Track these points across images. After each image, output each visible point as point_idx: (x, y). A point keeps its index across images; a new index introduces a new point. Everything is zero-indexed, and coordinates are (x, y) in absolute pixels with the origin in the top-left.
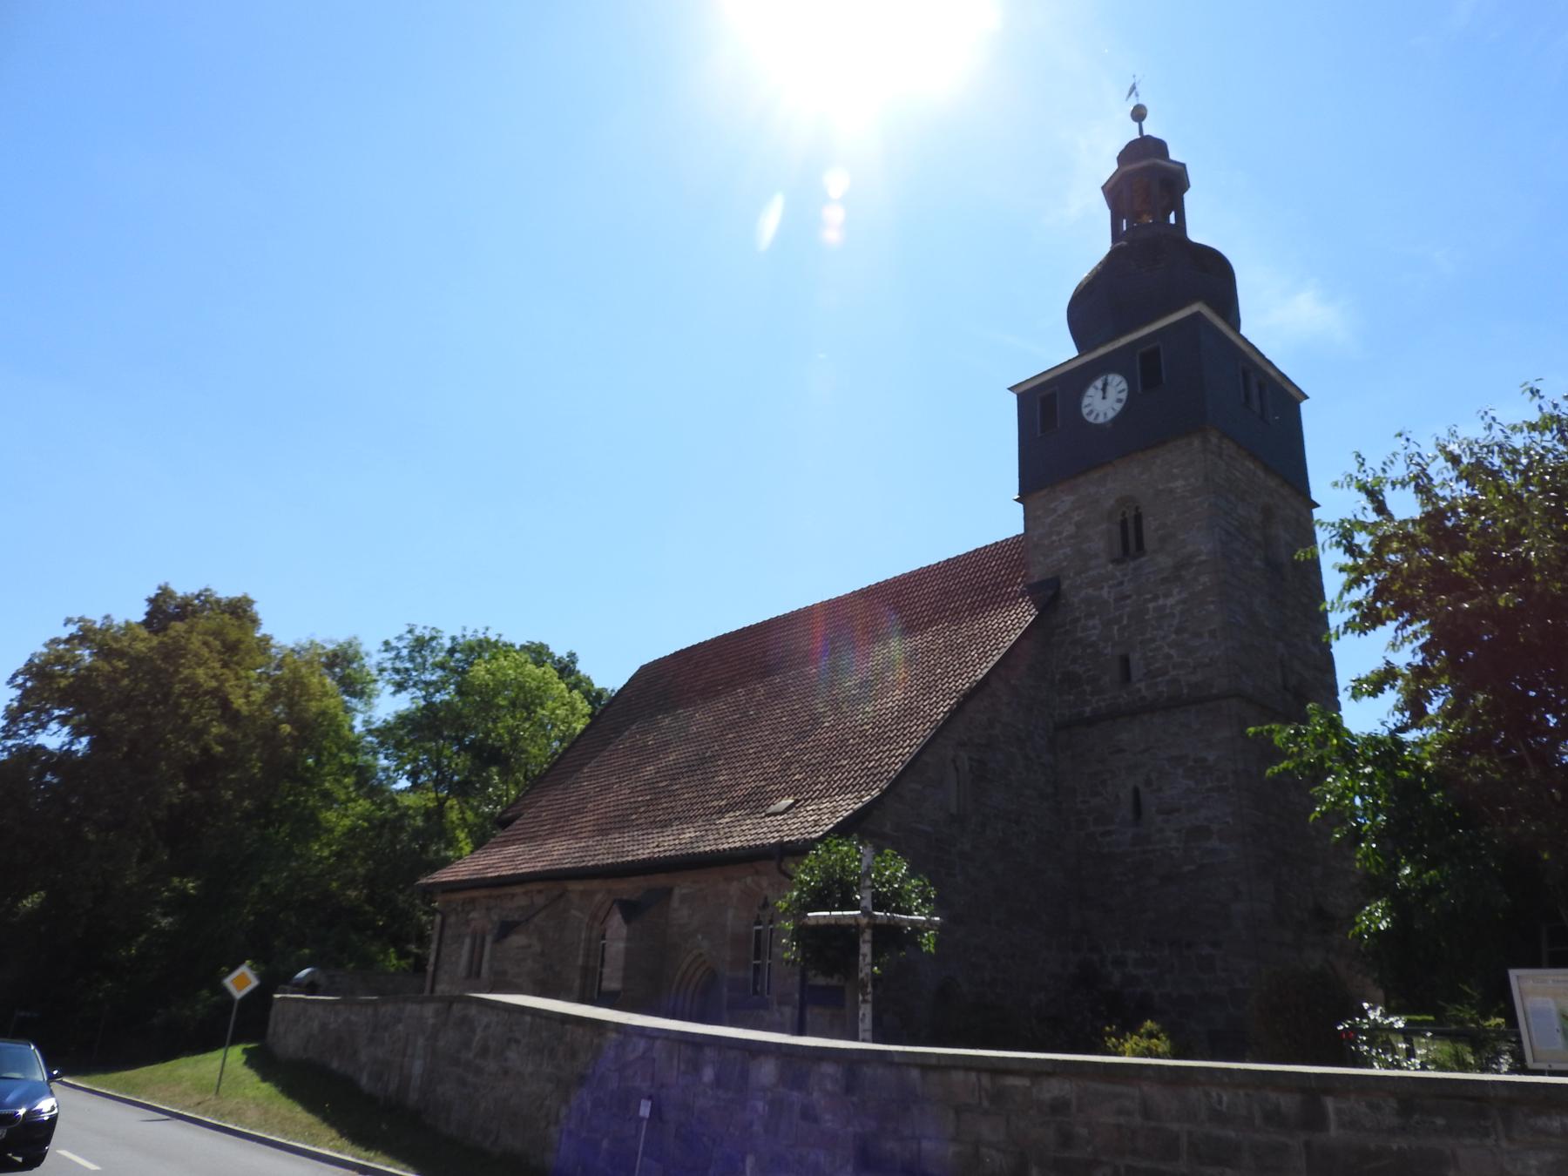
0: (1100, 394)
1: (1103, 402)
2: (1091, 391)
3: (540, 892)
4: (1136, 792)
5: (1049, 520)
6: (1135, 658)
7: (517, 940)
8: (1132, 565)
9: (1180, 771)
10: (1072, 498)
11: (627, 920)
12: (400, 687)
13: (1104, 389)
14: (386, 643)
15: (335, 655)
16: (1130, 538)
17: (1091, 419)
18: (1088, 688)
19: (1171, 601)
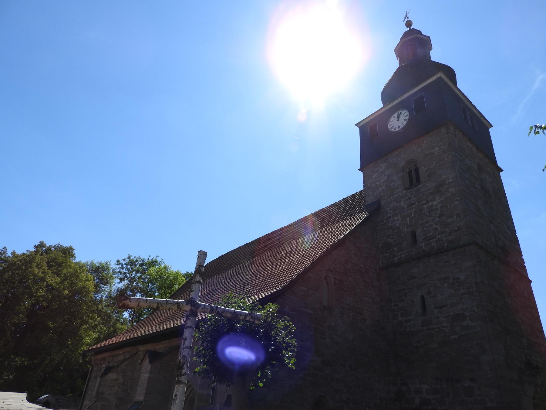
0: (396, 119)
1: (398, 123)
2: (392, 119)
3: (128, 352)
4: (423, 298)
5: (374, 176)
6: (419, 232)
7: (112, 376)
8: (415, 189)
9: (446, 285)
10: (385, 165)
11: (151, 362)
12: (121, 280)
13: (398, 117)
14: (118, 261)
15: (99, 268)
16: (413, 177)
17: (393, 130)
18: (396, 249)
19: (435, 203)
